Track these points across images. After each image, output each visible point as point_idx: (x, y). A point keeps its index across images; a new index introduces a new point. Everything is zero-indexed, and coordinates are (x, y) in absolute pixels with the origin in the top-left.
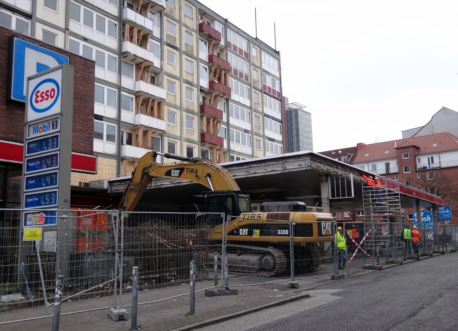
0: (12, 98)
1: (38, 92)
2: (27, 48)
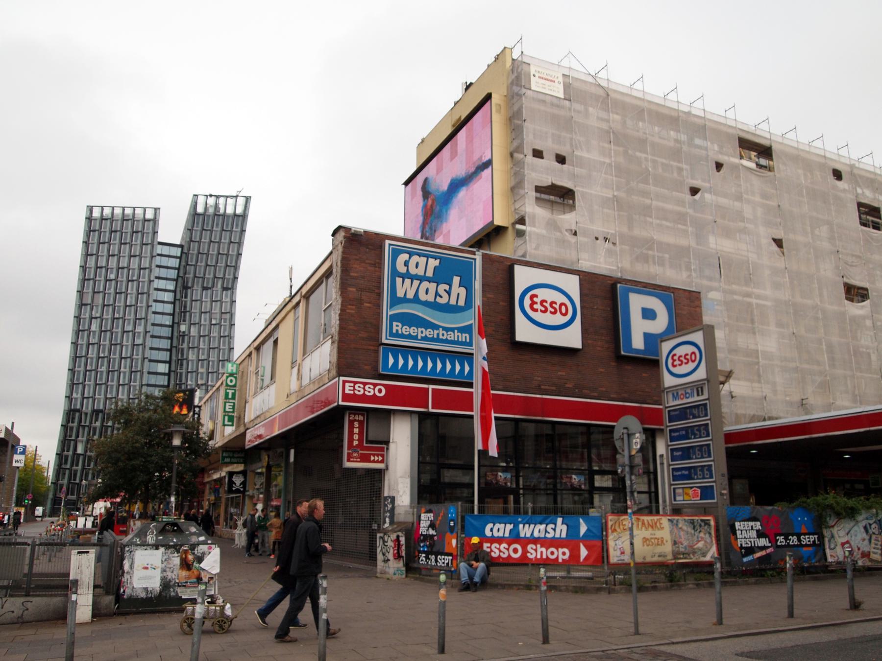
0: (623, 353)
1: (675, 355)
2: (444, 227)
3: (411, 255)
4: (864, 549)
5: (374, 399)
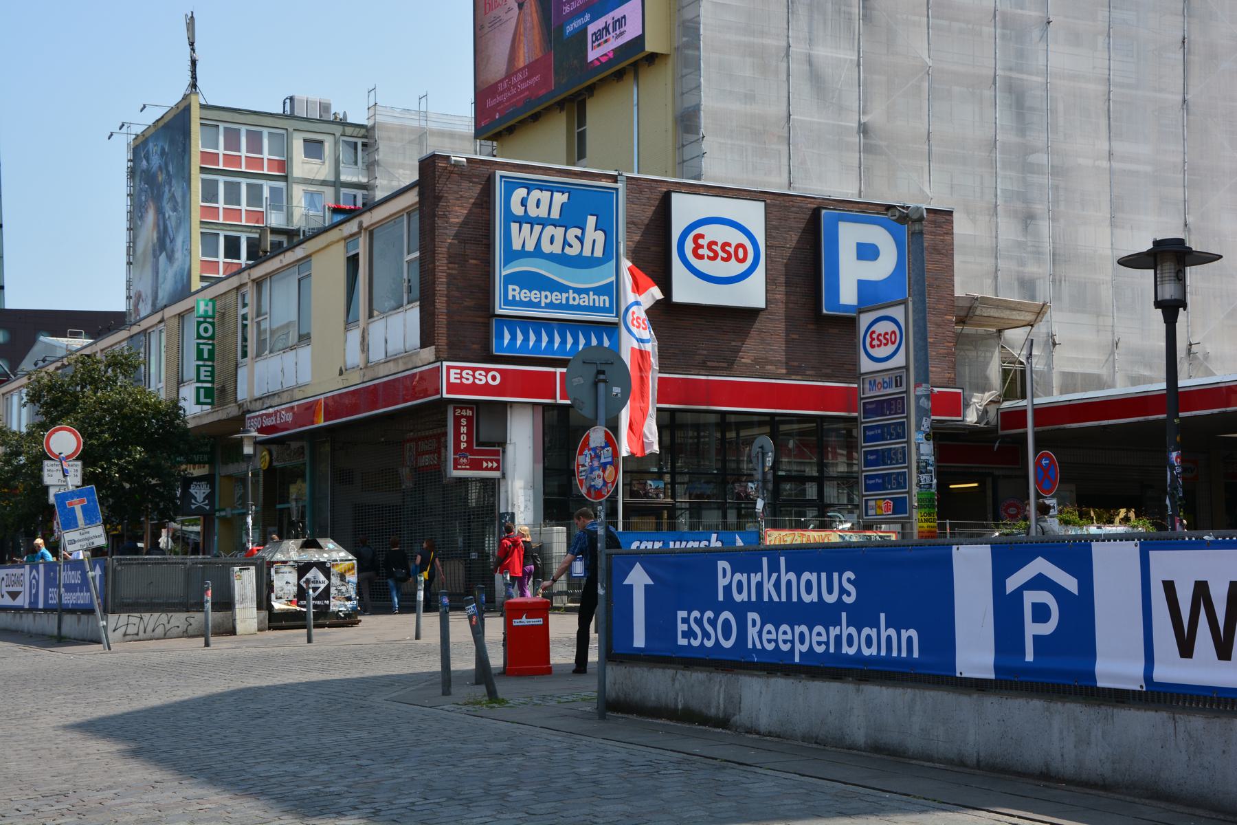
0: (825, 311)
1: (874, 332)
5: (486, 389)
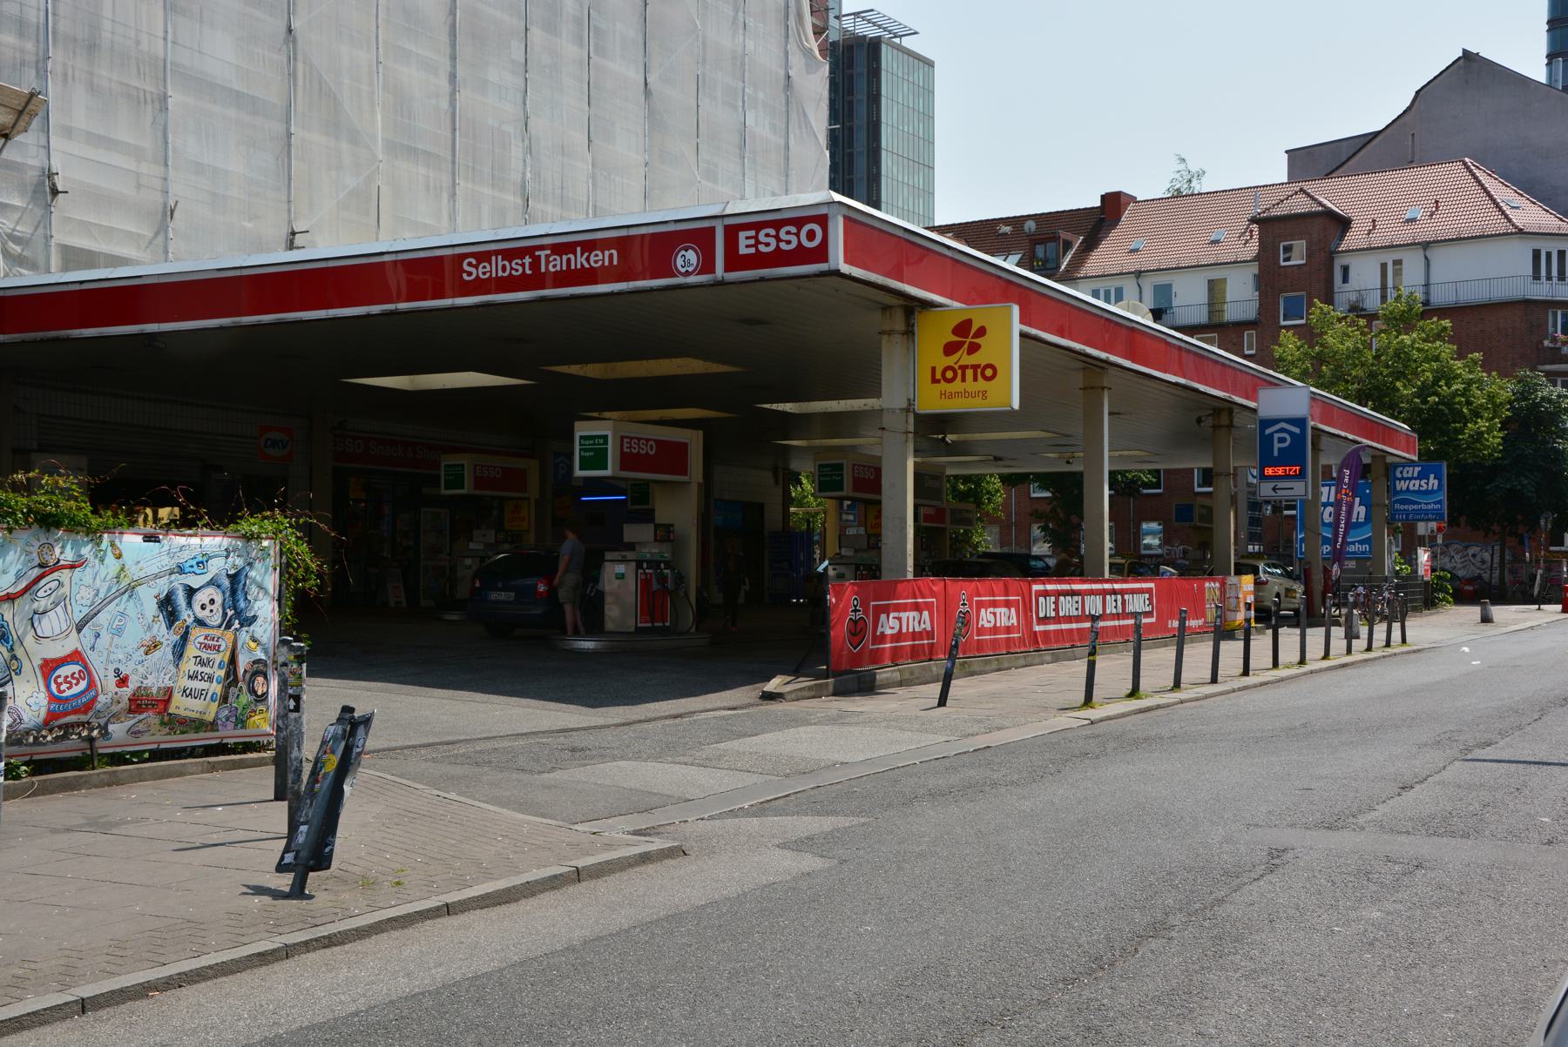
3: (1404, 467)
4: (148, 682)
